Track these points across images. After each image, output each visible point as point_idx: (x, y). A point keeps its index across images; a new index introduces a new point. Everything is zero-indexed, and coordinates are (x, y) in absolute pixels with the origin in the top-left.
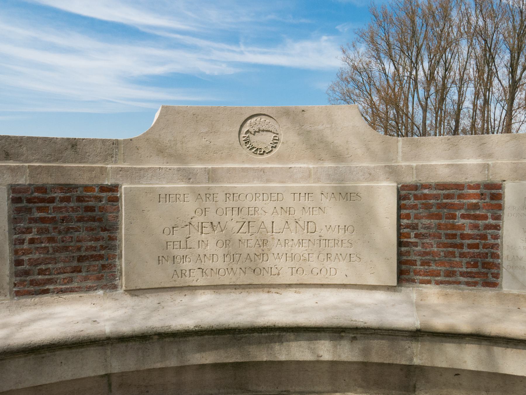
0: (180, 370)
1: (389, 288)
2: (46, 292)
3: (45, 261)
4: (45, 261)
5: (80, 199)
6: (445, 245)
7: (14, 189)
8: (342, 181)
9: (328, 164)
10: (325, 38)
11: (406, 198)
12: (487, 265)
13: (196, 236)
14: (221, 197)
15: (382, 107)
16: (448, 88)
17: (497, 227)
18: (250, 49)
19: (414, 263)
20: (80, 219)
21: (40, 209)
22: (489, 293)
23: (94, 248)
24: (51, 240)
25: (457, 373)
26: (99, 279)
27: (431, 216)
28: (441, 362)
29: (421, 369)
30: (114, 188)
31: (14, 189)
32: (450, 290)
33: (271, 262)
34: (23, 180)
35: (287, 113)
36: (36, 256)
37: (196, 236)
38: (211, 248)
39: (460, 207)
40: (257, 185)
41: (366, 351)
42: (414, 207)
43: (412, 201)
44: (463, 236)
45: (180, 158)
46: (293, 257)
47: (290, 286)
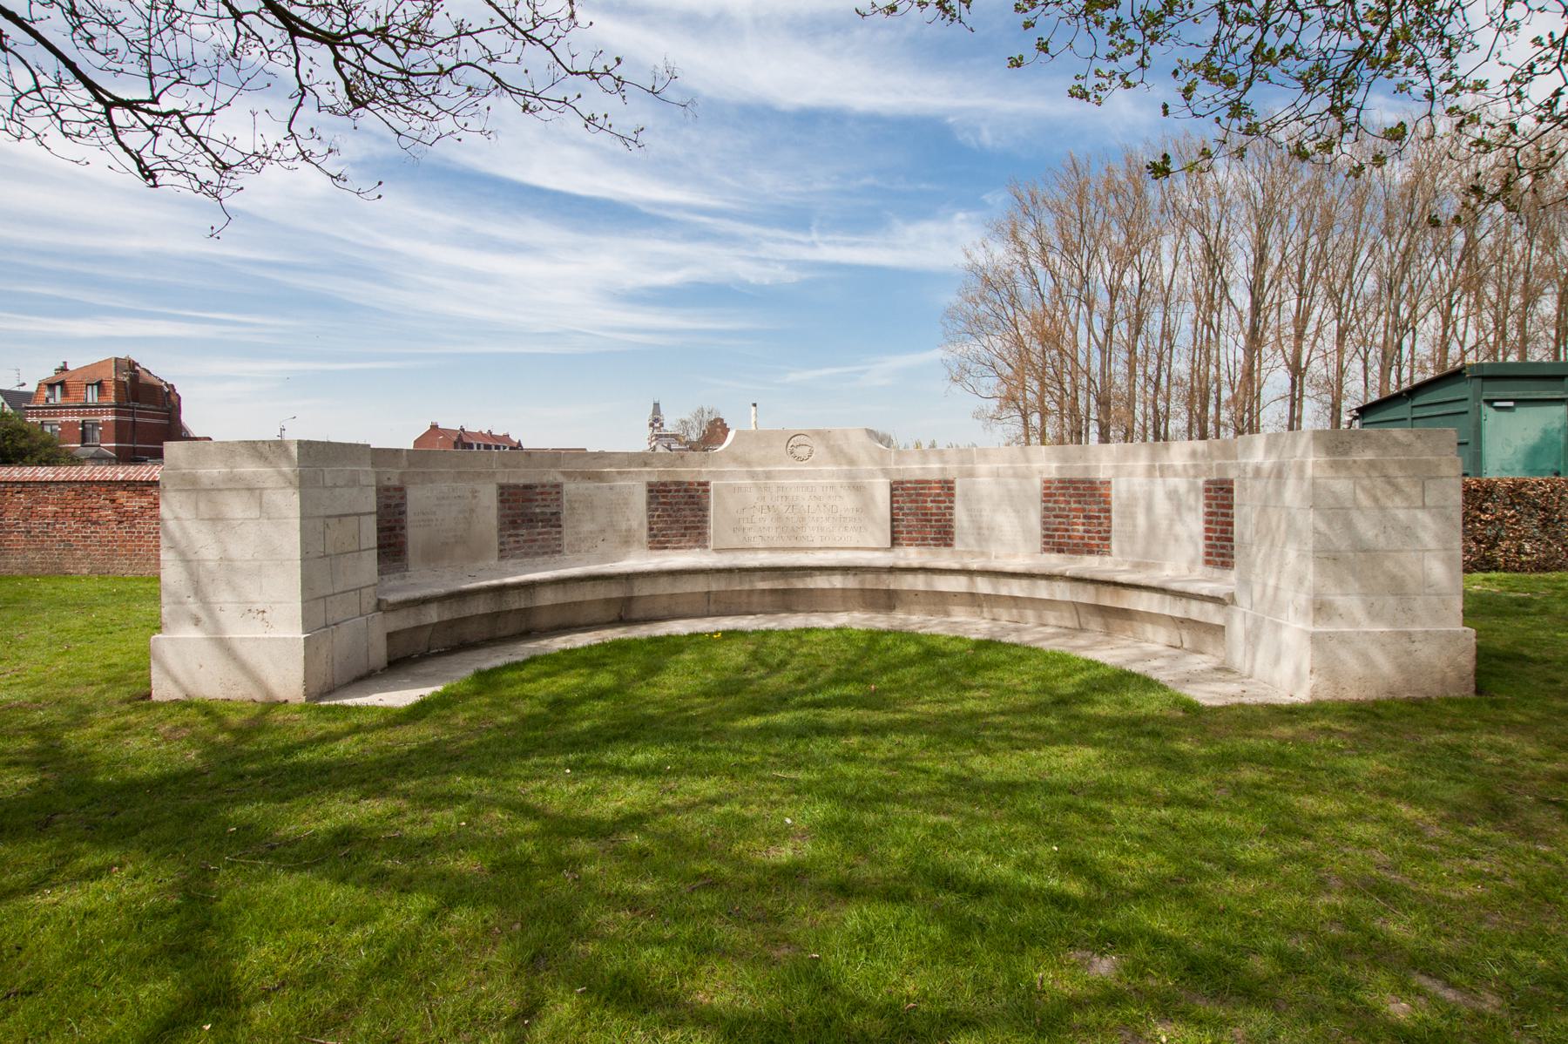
0: (751, 592)
1: (886, 549)
3: (665, 529)
4: (665, 529)
5: (686, 491)
6: (921, 520)
7: (649, 484)
8: (854, 478)
9: (845, 467)
10: (961, 216)
11: (897, 489)
12: (947, 533)
13: (758, 515)
14: (774, 489)
15: (1035, 346)
16: (1316, 233)
17: (951, 508)
18: (829, 238)
19: (902, 532)
20: (686, 503)
21: (663, 497)
24: (669, 516)
25: (916, 593)
26: (697, 541)
27: (911, 502)
28: (905, 587)
29: (895, 591)
30: (706, 484)
31: (649, 484)
32: (923, 549)
33: (808, 532)
34: (654, 479)
35: (818, 433)
37: (758, 515)
38: (768, 523)
39: (930, 495)
40: (797, 481)
41: (862, 582)
42: (902, 495)
43: (900, 492)
44: (932, 514)
45: (748, 464)
46: (822, 529)
47: (820, 548)
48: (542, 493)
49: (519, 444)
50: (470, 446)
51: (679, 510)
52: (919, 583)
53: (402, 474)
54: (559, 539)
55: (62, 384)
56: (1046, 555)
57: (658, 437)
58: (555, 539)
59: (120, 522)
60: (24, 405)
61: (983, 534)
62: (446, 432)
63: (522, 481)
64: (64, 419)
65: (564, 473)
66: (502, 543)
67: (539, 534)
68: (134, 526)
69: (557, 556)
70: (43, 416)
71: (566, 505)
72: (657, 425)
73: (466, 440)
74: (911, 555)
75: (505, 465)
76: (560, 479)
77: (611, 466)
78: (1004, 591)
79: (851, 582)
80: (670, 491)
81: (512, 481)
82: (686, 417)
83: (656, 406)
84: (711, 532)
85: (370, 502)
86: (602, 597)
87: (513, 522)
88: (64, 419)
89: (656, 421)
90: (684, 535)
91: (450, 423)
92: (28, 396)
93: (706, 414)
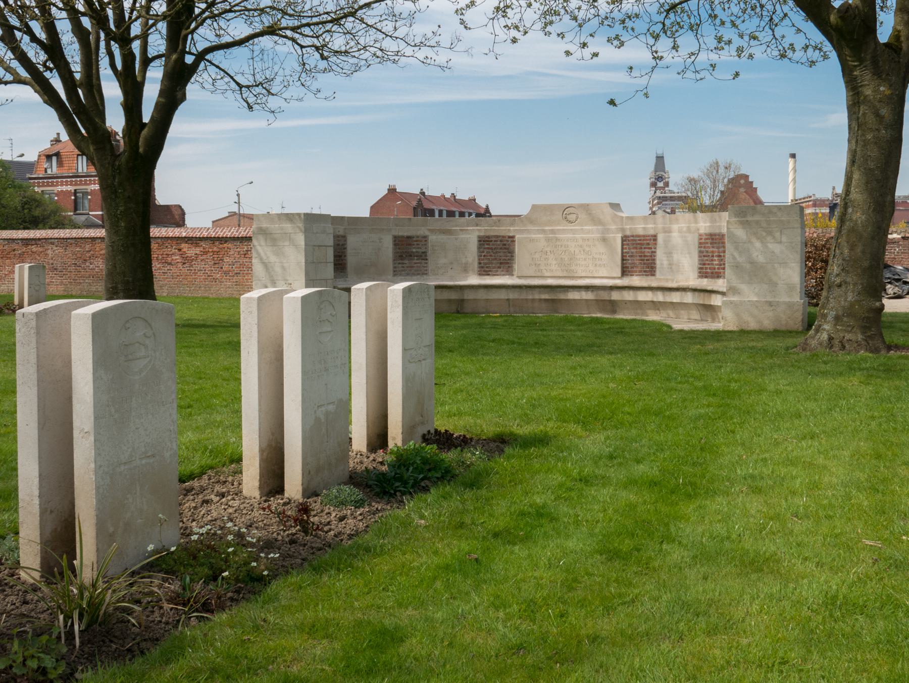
0: (533, 300)
2: (489, 275)
20: (501, 249)
21: (487, 244)
22: (653, 278)
23: (505, 260)
24: (491, 256)
25: (626, 302)
30: (513, 237)
31: (479, 237)
34: (482, 234)
36: (485, 261)
48: (417, 241)
49: (487, 210)
50: (431, 213)
51: (496, 252)
52: (629, 296)
53: (345, 229)
54: (426, 267)
55: (57, 154)
56: (700, 280)
57: (662, 199)
58: (424, 267)
59: (184, 263)
60: (28, 176)
61: (673, 267)
62: (405, 196)
63: (406, 234)
64: (59, 188)
65: (429, 230)
66: (395, 267)
67: (415, 263)
68: (191, 266)
69: (425, 276)
70: (43, 186)
71: (430, 248)
72: (660, 184)
73: (427, 205)
74: (636, 280)
75: (397, 225)
76: (427, 233)
77: (456, 226)
78: (668, 299)
79: (589, 296)
80: (491, 241)
81: (401, 234)
82: (695, 175)
83: (660, 160)
84: (516, 266)
85: (330, 241)
86: (446, 298)
87: (401, 256)
88: (59, 188)
89: (659, 179)
90: (499, 267)
91: (409, 186)
92: (30, 166)
93: (721, 170)
